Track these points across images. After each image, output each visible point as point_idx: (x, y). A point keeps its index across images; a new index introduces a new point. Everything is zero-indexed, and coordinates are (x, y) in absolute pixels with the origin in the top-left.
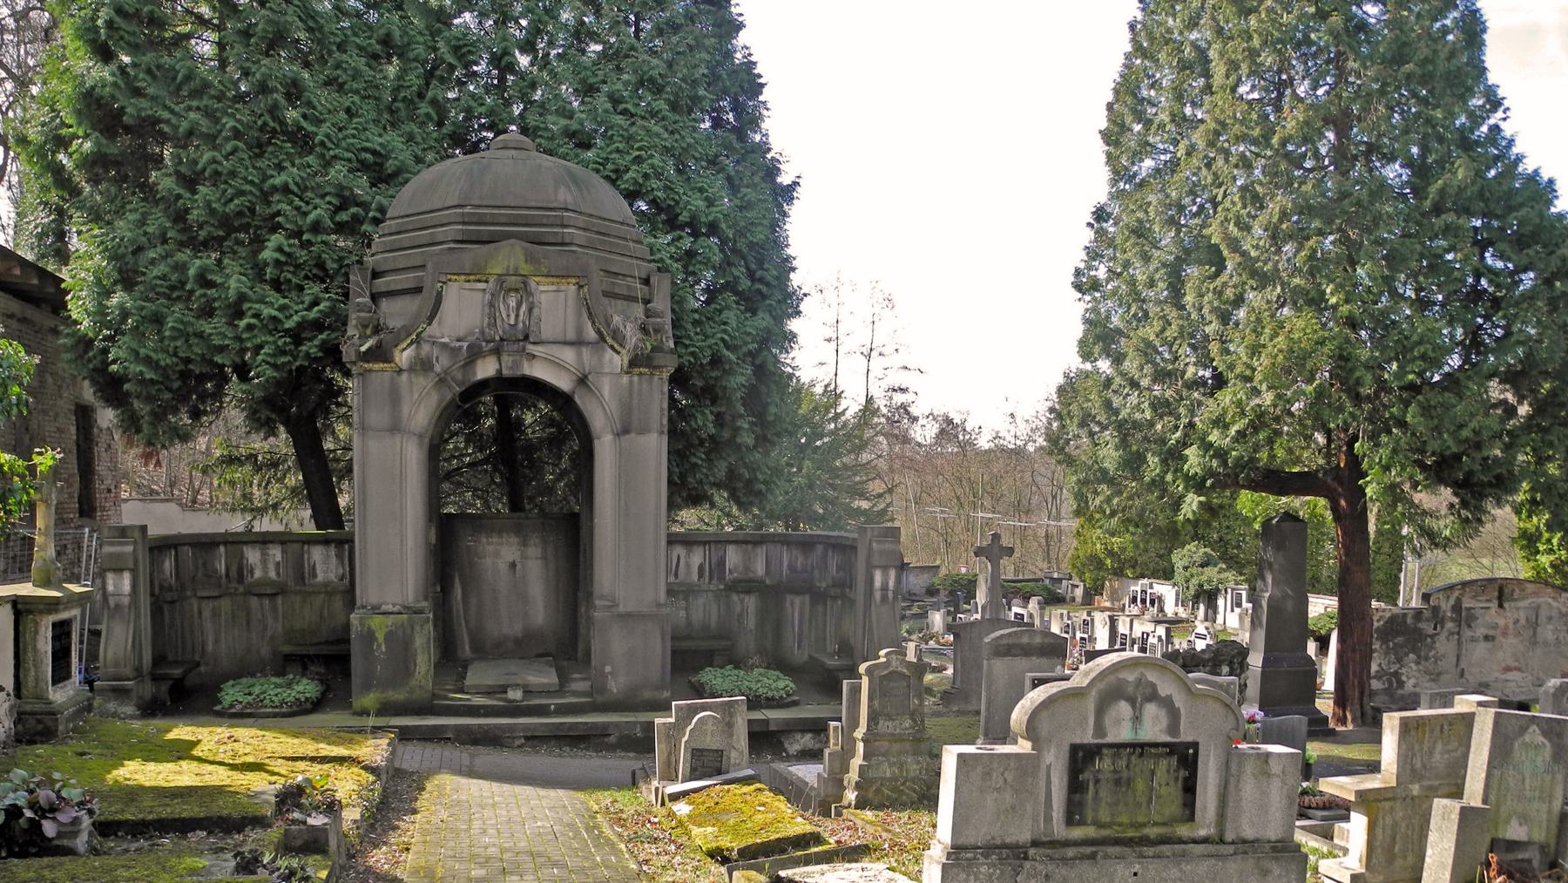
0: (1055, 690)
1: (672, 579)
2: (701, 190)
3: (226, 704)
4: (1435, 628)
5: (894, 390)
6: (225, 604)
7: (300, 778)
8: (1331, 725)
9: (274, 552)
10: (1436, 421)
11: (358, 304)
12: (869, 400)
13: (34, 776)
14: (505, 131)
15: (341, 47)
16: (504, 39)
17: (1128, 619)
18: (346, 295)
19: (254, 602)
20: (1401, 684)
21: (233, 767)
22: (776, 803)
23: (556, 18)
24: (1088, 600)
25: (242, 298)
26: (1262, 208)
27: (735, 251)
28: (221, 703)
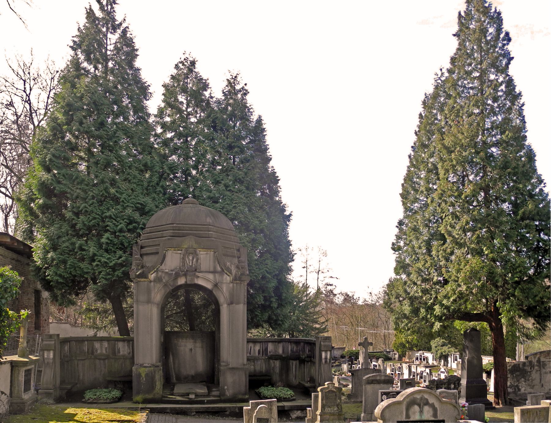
0: (391, 402)
1: (249, 355)
2: (257, 218)
3: (87, 399)
4: (531, 369)
5: (327, 285)
8: (494, 405)
10: (526, 294)
11: (136, 258)
12: (319, 289)
14: (187, 197)
15: (130, 167)
16: (187, 165)
17: (415, 366)
19: (97, 361)
20: (519, 390)
24: (400, 358)
25: (95, 255)
26: (459, 220)
28: (85, 398)
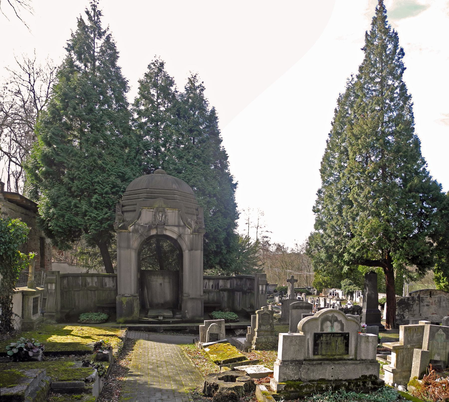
1: (205, 288)
2: (211, 185)
7: (101, 340)
11: (118, 214)
19: (89, 292)
21: (82, 337)
23: (171, 138)
25: (86, 211)
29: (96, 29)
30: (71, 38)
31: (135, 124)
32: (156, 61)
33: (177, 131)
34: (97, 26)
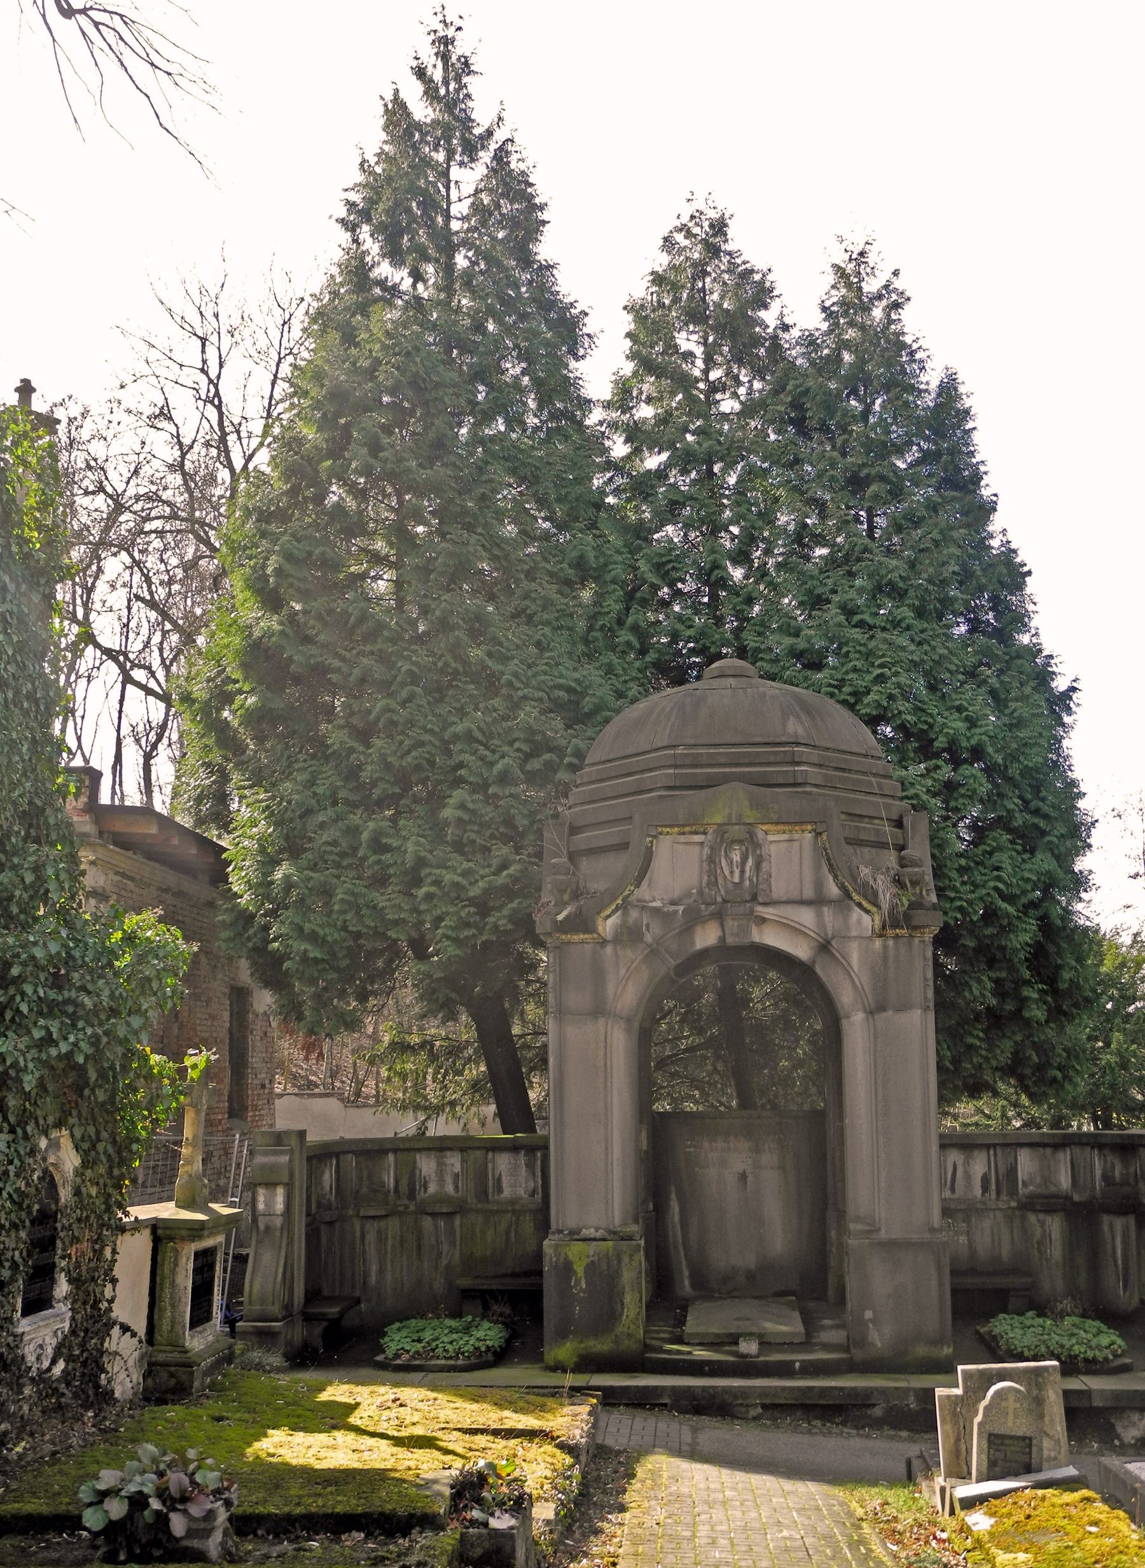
1: (947, 1194)
2: (960, 709)
3: (390, 1353)
6: (393, 1226)
7: (481, 1463)
9: (452, 1160)
11: (554, 865)
13: (165, 1454)
14: (719, 656)
16: (713, 551)
18: (539, 855)
19: (427, 1222)
21: (398, 1442)
22: (1115, 1523)
23: (771, 522)
25: (421, 862)
27: (1009, 780)
29: (454, 129)
30: (360, 178)
31: (619, 481)
32: (692, 217)
33: (795, 489)
34: (457, 119)
